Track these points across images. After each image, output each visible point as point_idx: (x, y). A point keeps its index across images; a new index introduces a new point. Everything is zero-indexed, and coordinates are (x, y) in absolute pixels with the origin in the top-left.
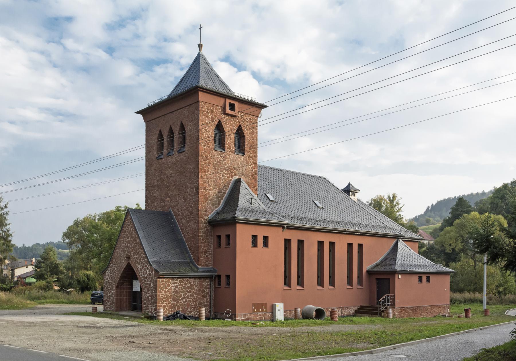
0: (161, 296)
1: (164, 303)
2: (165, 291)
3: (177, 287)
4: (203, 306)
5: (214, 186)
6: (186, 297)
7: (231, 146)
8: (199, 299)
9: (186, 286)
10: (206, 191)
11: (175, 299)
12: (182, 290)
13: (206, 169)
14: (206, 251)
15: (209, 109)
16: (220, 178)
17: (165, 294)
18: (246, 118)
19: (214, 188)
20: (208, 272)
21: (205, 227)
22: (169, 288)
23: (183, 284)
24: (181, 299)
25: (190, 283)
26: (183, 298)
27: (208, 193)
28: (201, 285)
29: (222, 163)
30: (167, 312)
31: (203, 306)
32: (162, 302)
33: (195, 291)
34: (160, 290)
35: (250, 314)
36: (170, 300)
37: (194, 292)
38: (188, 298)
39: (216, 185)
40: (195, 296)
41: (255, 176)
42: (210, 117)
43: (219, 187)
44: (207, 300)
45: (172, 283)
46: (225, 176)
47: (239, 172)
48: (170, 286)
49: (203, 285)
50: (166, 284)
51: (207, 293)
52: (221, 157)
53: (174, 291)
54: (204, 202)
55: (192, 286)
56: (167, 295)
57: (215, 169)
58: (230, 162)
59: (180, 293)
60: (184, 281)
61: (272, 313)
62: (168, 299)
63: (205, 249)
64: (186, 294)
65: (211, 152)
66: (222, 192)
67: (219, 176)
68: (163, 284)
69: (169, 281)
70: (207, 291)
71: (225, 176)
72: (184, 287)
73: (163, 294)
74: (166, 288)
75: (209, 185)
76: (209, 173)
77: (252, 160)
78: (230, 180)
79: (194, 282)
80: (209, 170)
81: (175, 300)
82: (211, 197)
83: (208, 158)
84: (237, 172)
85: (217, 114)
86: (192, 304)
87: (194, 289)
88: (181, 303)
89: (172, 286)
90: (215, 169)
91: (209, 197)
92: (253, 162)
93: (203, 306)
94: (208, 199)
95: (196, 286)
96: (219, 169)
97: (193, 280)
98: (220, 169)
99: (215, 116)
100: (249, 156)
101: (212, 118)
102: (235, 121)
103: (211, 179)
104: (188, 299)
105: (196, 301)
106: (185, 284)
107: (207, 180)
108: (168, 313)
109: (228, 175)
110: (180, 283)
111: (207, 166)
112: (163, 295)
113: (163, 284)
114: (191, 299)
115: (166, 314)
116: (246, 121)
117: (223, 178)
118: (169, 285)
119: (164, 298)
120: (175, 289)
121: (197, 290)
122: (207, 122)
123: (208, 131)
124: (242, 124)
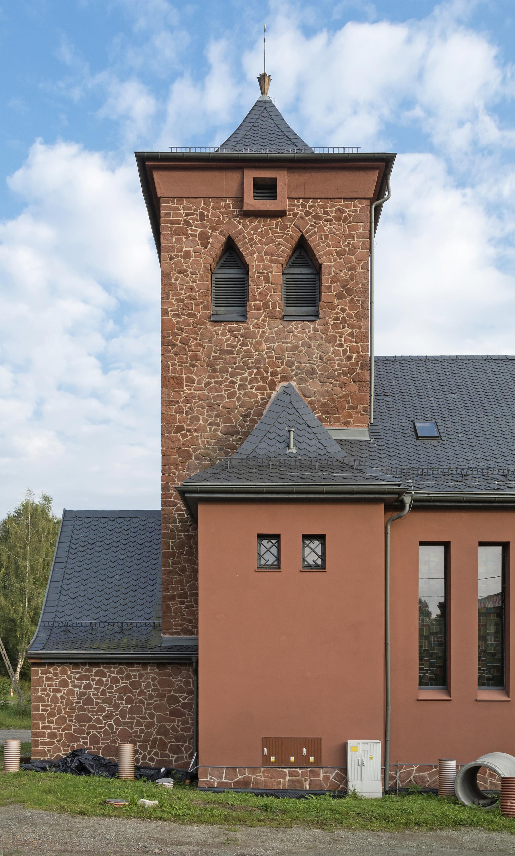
0: (43, 710)
1: (50, 728)
2: (55, 697)
3: (88, 687)
4: (172, 738)
5: (210, 420)
6: (116, 715)
7: (268, 301)
8: (160, 719)
9: (116, 687)
10: (184, 436)
11: (81, 720)
12: (105, 695)
13: (184, 376)
14: (186, 593)
15: (193, 214)
16: (231, 395)
17: (56, 706)
18: (325, 212)
19: (211, 424)
20: (181, 648)
21: (180, 531)
22: (65, 690)
23: (107, 681)
24: (101, 718)
25: (128, 677)
26: (108, 717)
27: (191, 438)
28: (166, 684)
29: (239, 352)
30: (60, 749)
31: (172, 738)
32: (47, 724)
33: (146, 699)
34: (39, 694)
35: (254, 770)
36: (70, 721)
37: (141, 701)
38: (123, 716)
39: (217, 416)
40: (145, 713)
41: (358, 374)
42: (195, 236)
43: (228, 420)
44: (184, 722)
45: (75, 678)
46: (249, 386)
47: (298, 368)
48: (67, 686)
49: (170, 684)
50: (57, 679)
51: (184, 706)
52: (235, 336)
53: (81, 699)
54: (177, 465)
55: (135, 685)
56: (59, 706)
57: (214, 371)
58: (264, 346)
59: (97, 704)
60: (113, 672)
61: (340, 770)
62: (64, 717)
63: (182, 589)
64: (117, 706)
65: (201, 328)
66: (237, 433)
67: (226, 390)
68: (48, 679)
69: (66, 673)
70: (184, 699)
71: (249, 386)
72: (111, 687)
73: (48, 706)
74: (58, 691)
75: (197, 419)
76: (195, 385)
77: (346, 328)
78: (265, 396)
79: (141, 676)
80: (194, 377)
81: (84, 722)
82: (199, 449)
83: (191, 346)
84: (292, 371)
85: (219, 223)
86: (136, 732)
87: (142, 693)
88: (101, 728)
89: (75, 686)
90: (214, 371)
91: (195, 450)
92: (351, 335)
93: (173, 740)
94: (190, 456)
95: (148, 686)
96: (227, 371)
97: (138, 670)
98: (230, 369)
99: (213, 229)
100: (337, 319)
101: (204, 236)
102: (283, 228)
103: (202, 400)
104: (124, 718)
105: (150, 725)
106: (115, 681)
107: (189, 405)
108: (63, 753)
109: (261, 384)
110: (97, 678)
111: (187, 368)
112: (49, 708)
113: (48, 679)
114: (134, 718)
115: (58, 756)
116: (325, 220)
117: (242, 392)
118: (64, 684)
119: (51, 715)
120: (82, 694)
121: (151, 697)
122: (185, 249)
123: (191, 273)
124: (308, 231)
